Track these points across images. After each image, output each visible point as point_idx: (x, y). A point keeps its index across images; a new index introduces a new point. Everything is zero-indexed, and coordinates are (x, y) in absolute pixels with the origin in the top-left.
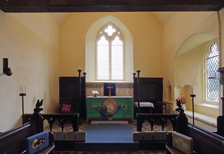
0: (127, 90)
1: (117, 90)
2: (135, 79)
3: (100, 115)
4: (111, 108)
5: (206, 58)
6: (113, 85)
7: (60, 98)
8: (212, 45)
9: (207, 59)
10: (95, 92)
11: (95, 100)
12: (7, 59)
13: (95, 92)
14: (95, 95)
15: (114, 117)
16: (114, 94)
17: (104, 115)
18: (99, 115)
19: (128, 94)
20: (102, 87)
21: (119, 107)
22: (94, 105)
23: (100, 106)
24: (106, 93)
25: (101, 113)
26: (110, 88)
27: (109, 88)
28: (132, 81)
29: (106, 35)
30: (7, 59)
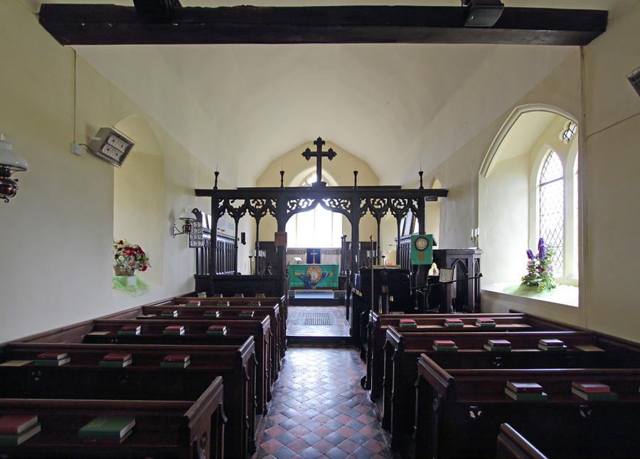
0: (335, 256)
1: (323, 257)
2: (345, 244)
3: (303, 283)
4: (315, 275)
5: (538, 184)
6: (318, 251)
7: (325, 260)
8: (547, 160)
9: (541, 185)
10: (298, 259)
11: (298, 266)
12: (244, 233)
13: (298, 259)
14: (298, 262)
15: (318, 285)
16: (318, 261)
17: (308, 285)
18: (301, 284)
19: (335, 260)
20: (133, 269)
21: (324, 275)
22: (297, 274)
23: (303, 274)
24: (309, 260)
25: (304, 282)
26: (314, 254)
27: (313, 256)
28: (338, 245)
29: (231, 209)
30: (244, 233)
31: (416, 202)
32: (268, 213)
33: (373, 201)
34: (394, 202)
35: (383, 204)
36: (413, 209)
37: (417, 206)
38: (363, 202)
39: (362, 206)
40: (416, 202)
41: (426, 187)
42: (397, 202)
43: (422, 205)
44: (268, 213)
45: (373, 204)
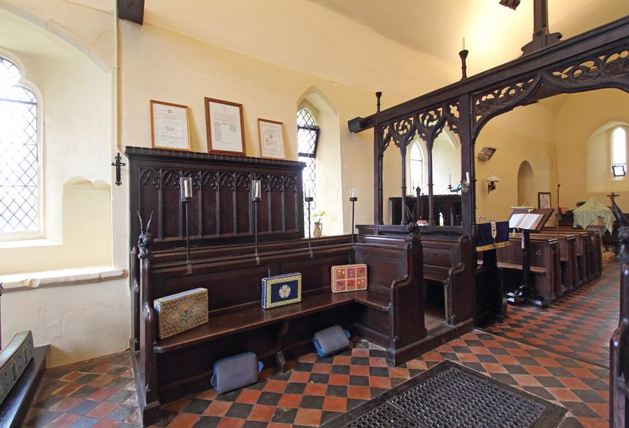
31: (456, 108)
34: (423, 118)
35: (409, 126)
37: (457, 114)
38: (386, 131)
39: (385, 136)
40: (456, 108)
41: (253, 153)
42: (427, 117)
45: (398, 130)
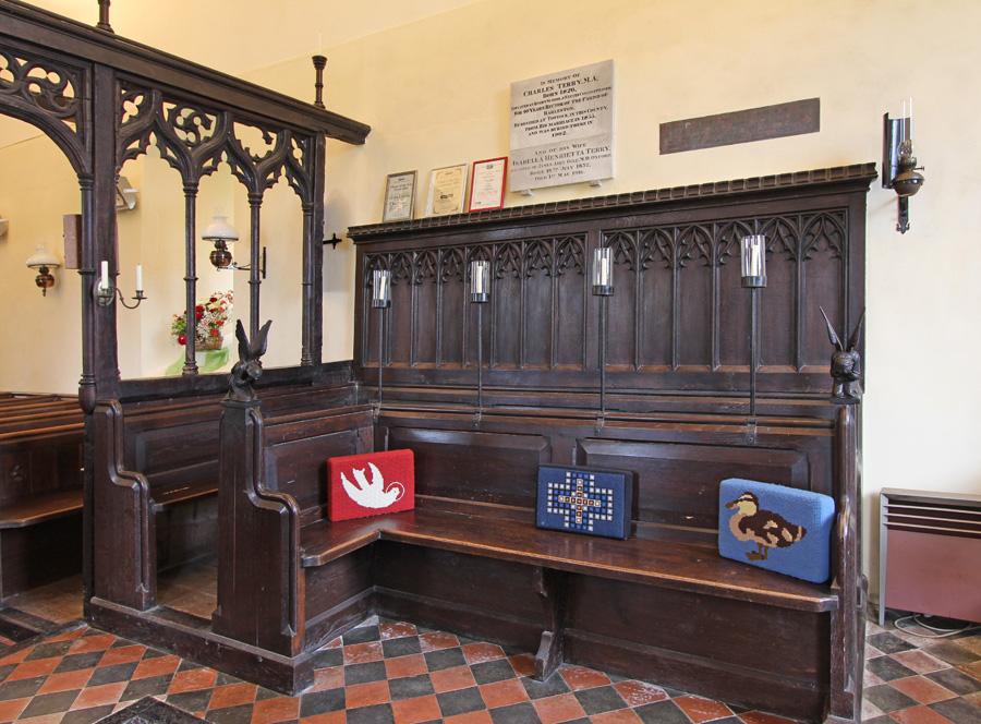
29: (239, 158)
32: (283, 179)
33: (174, 113)
35: (204, 133)
36: (294, 170)
43: (316, 157)
44: (283, 179)
